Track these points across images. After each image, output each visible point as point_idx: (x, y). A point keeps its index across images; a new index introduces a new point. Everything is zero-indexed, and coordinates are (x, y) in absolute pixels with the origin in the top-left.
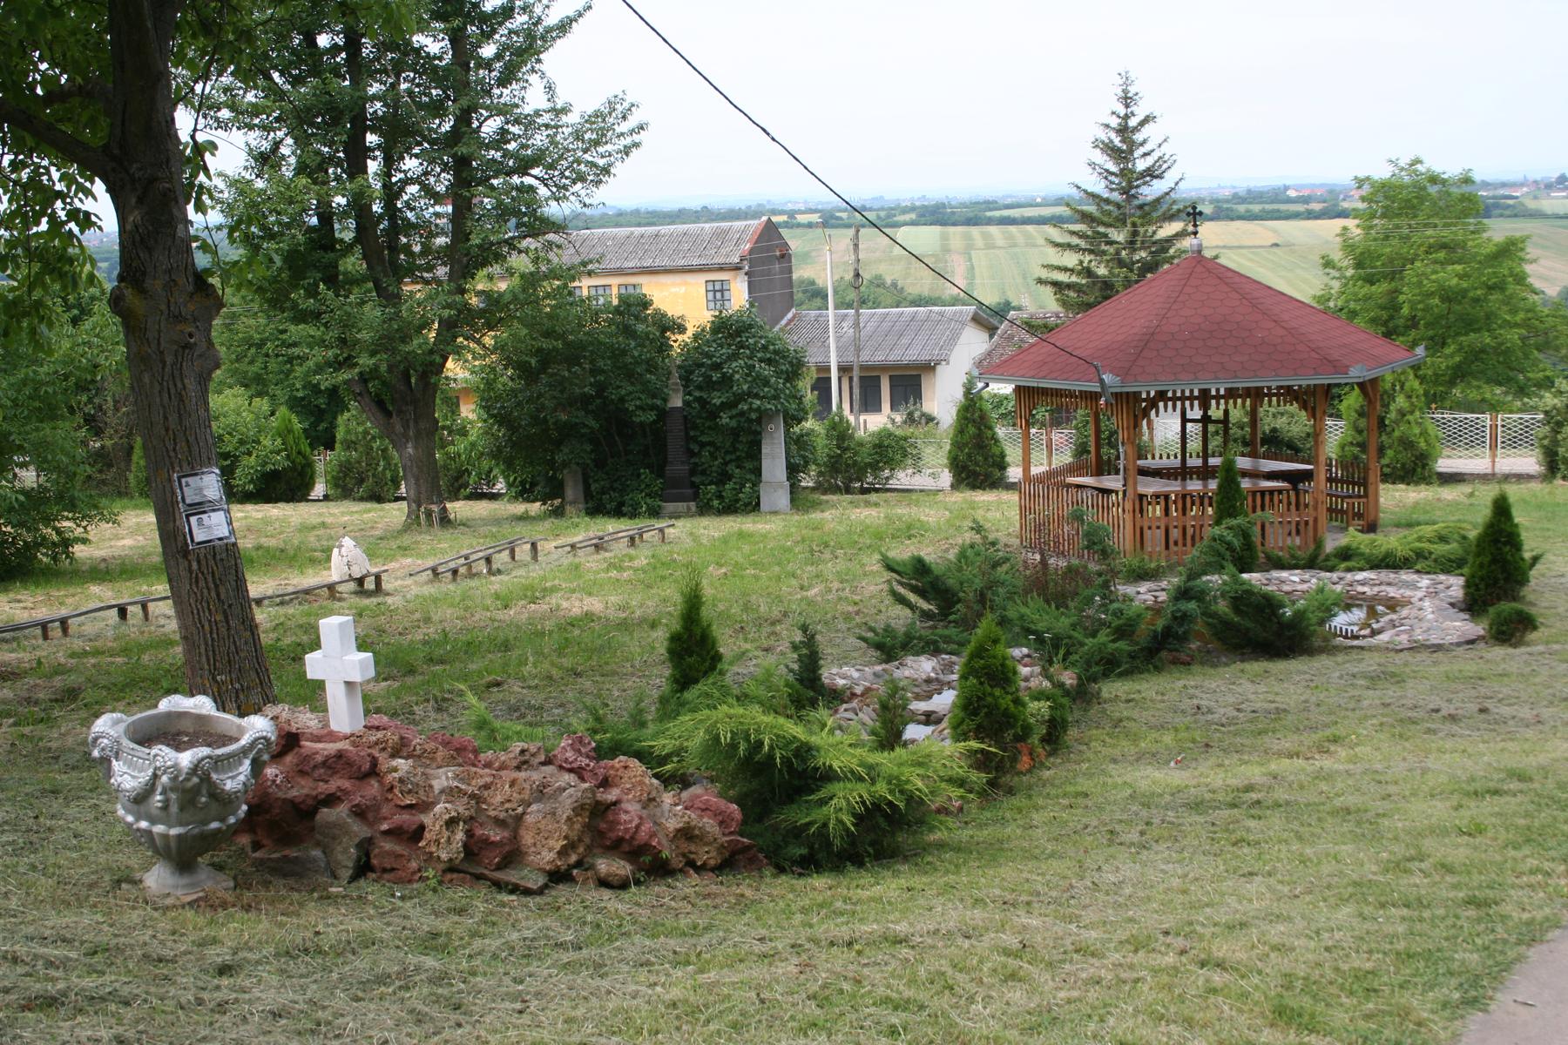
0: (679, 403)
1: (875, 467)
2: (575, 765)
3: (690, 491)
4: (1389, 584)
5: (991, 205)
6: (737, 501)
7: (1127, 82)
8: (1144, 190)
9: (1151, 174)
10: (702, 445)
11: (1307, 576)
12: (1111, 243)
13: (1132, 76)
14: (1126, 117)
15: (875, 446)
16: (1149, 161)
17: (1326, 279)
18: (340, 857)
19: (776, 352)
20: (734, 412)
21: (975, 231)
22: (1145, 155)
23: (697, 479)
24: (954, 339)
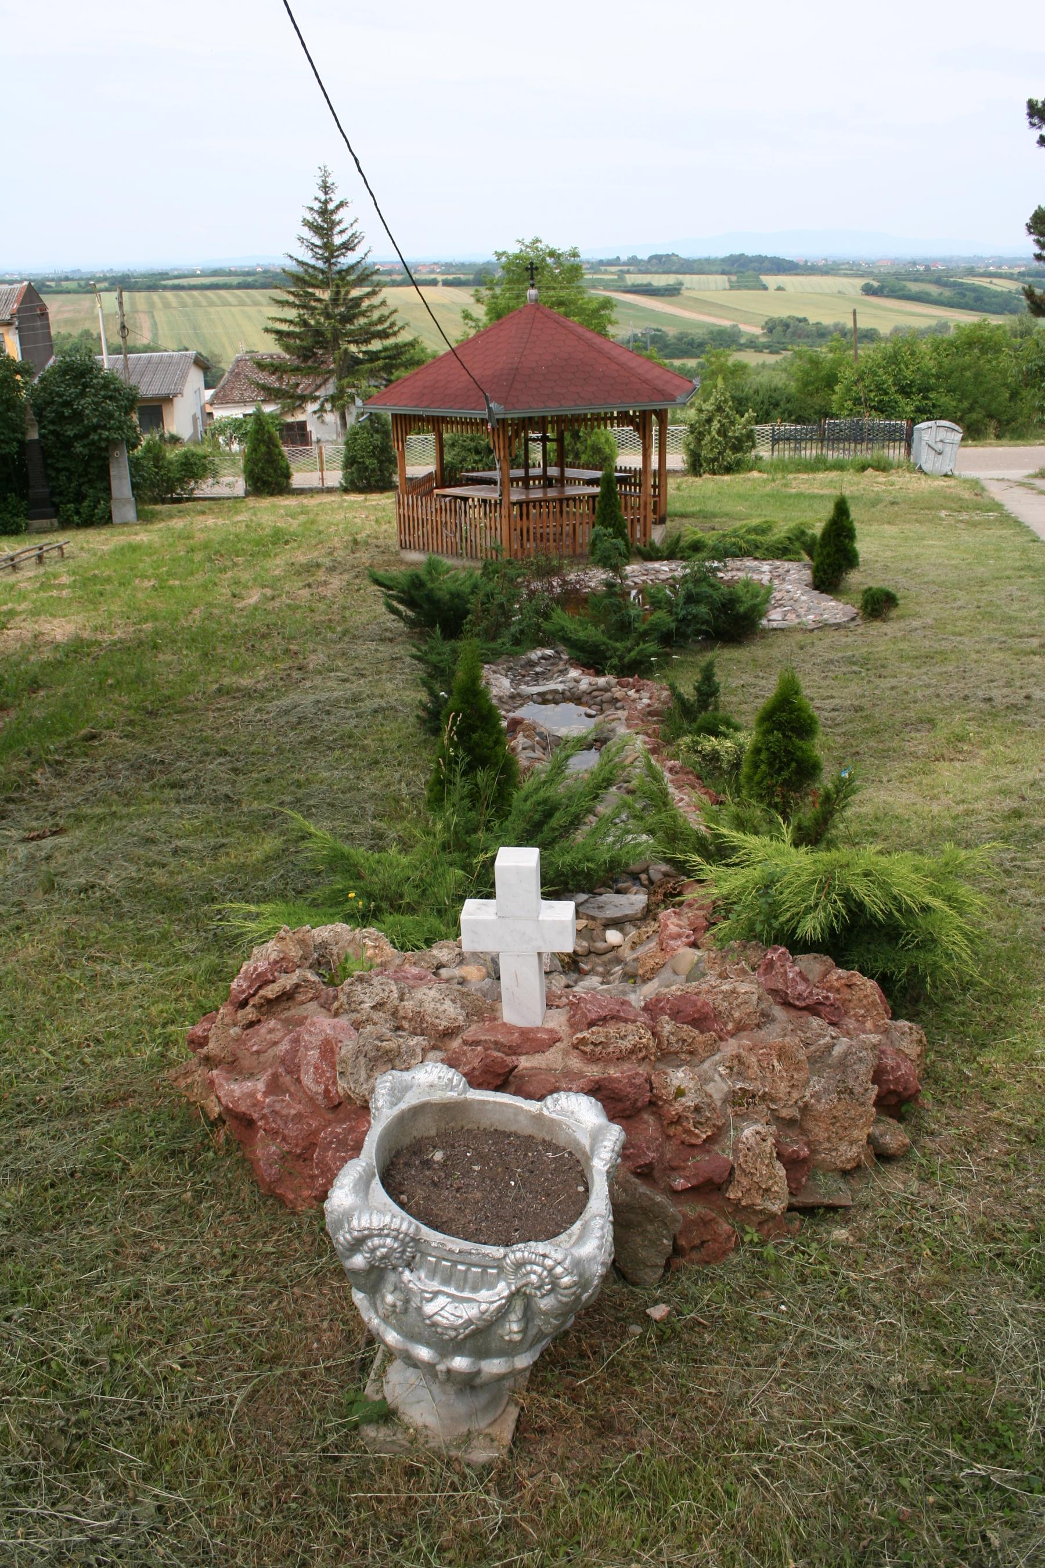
0: (36, 436)
1: (181, 481)
2: (809, 1002)
3: (51, 510)
4: (738, 570)
5: (164, 275)
6: (93, 516)
7: (326, 174)
8: (341, 259)
9: (347, 247)
10: (58, 471)
11: (673, 566)
12: (319, 300)
13: (329, 170)
14: (326, 202)
15: (182, 464)
16: (345, 237)
17: (466, 329)
18: (643, 1254)
19: (116, 390)
20: (86, 441)
21: (155, 296)
22: (342, 232)
23: (56, 499)
24: (184, 377)
